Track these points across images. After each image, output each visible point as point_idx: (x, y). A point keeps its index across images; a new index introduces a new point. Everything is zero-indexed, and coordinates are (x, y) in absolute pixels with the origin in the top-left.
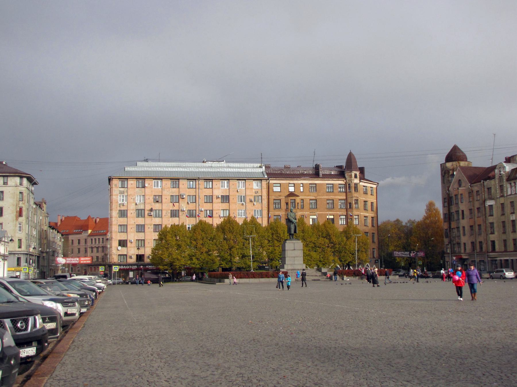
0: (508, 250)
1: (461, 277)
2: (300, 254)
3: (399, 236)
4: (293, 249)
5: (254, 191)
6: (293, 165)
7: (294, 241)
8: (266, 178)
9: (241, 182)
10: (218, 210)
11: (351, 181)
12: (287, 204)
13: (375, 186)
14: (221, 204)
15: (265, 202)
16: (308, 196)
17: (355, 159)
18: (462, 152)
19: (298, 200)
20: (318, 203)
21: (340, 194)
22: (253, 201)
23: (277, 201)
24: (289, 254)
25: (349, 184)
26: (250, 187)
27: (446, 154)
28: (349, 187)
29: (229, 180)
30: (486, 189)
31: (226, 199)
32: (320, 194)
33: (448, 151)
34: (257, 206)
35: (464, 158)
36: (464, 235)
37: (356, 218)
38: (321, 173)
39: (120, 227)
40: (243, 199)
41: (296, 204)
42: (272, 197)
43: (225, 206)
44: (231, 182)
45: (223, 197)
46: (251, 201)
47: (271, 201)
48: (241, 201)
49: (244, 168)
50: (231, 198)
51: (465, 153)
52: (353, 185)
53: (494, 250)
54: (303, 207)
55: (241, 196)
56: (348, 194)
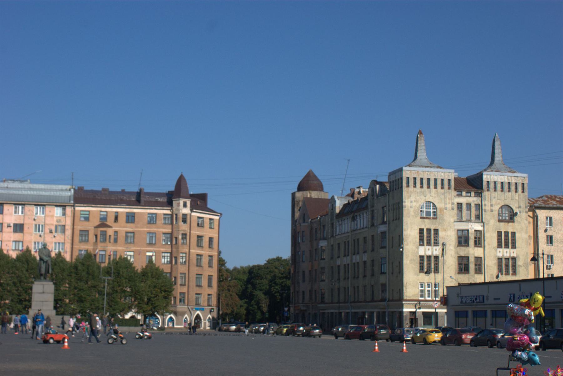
0: (375, 299)
1: (523, 327)
2: (50, 298)
3: (164, 279)
4: (41, 291)
5: (55, 219)
6: (113, 188)
7: (44, 283)
8: (72, 203)
9: (40, 208)
10: (9, 241)
11: (179, 210)
12: (96, 236)
13: (217, 218)
14: (3, 233)
15: (69, 232)
16: (124, 227)
17: (186, 185)
18: (318, 180)
19: (110, 232)
20: (136, 236)
21: (165, 226)
22: (54, 231)
23: (84, 233)
24: (36, 297)
25: (176, 215)
26: (51, 214)
27: (298, 183)
28: (176, 218)
29: (24, 205)
30: (322, 227)
31: (19, 228)
32: (139, 225)
33: (300, 179)
34: (59, 237)
35: (320, 188)
36: (304, 281)
37: (183, 257)
38: (142, 199)
39: (202, 245)
40: (38, 228)
41: (108, 237)
42: (78, 227)
43: (18, 236)
44: (27, 208)
45: (15, 225)
46: (51, 232)
47: (77, 233)
48: (39, 231)
49: (50, 190)
50: (26, 228)
51: (322, 181)
52: (180, 216)
53: (323, 302)
54: (116, 241)
55: (39, 225)
56: (174, 226)
